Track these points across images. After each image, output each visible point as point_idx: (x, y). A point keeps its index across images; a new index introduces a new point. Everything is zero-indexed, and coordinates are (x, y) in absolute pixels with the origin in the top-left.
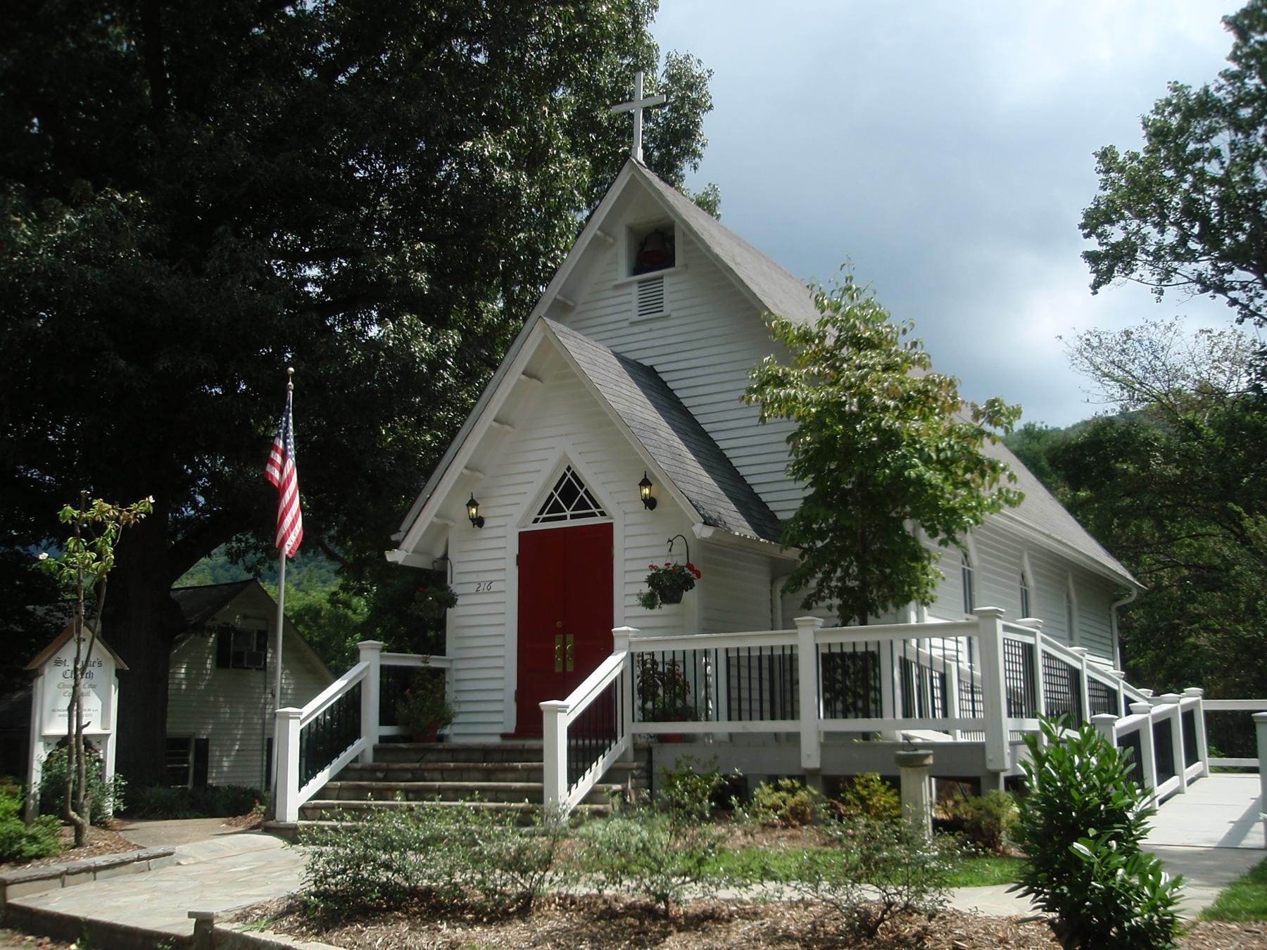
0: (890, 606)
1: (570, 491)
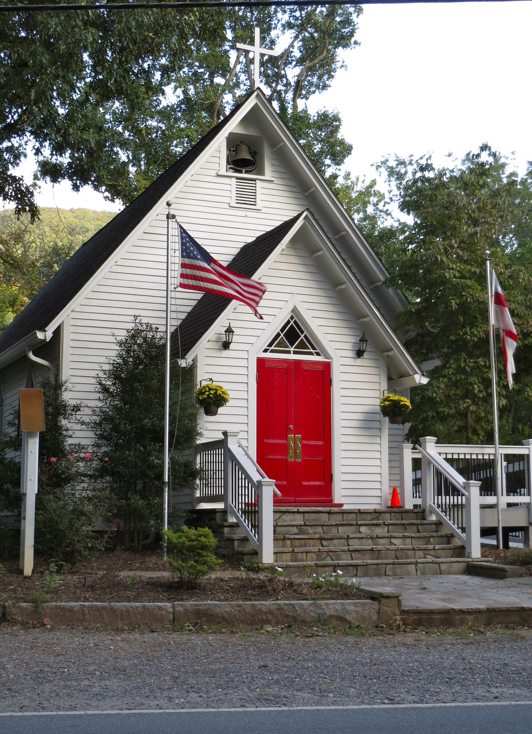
0: (120, 361)
1: (293, 333)
